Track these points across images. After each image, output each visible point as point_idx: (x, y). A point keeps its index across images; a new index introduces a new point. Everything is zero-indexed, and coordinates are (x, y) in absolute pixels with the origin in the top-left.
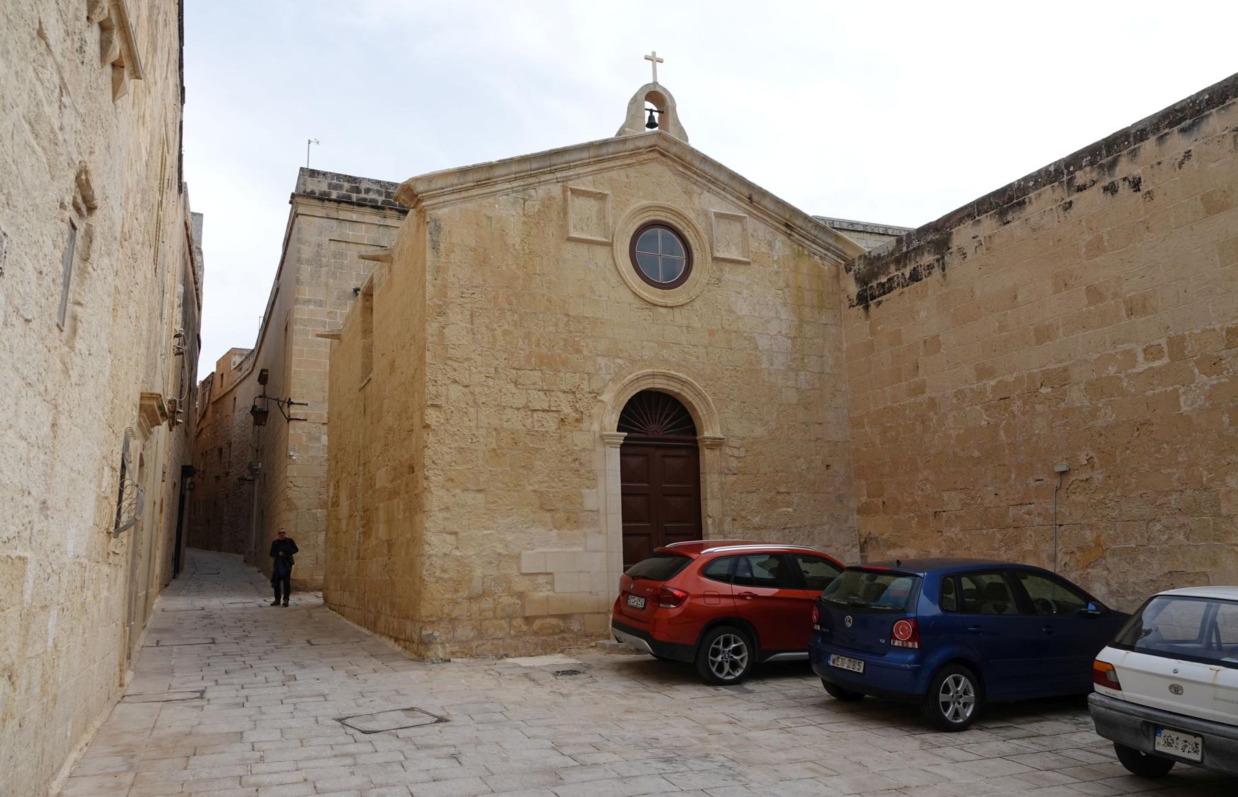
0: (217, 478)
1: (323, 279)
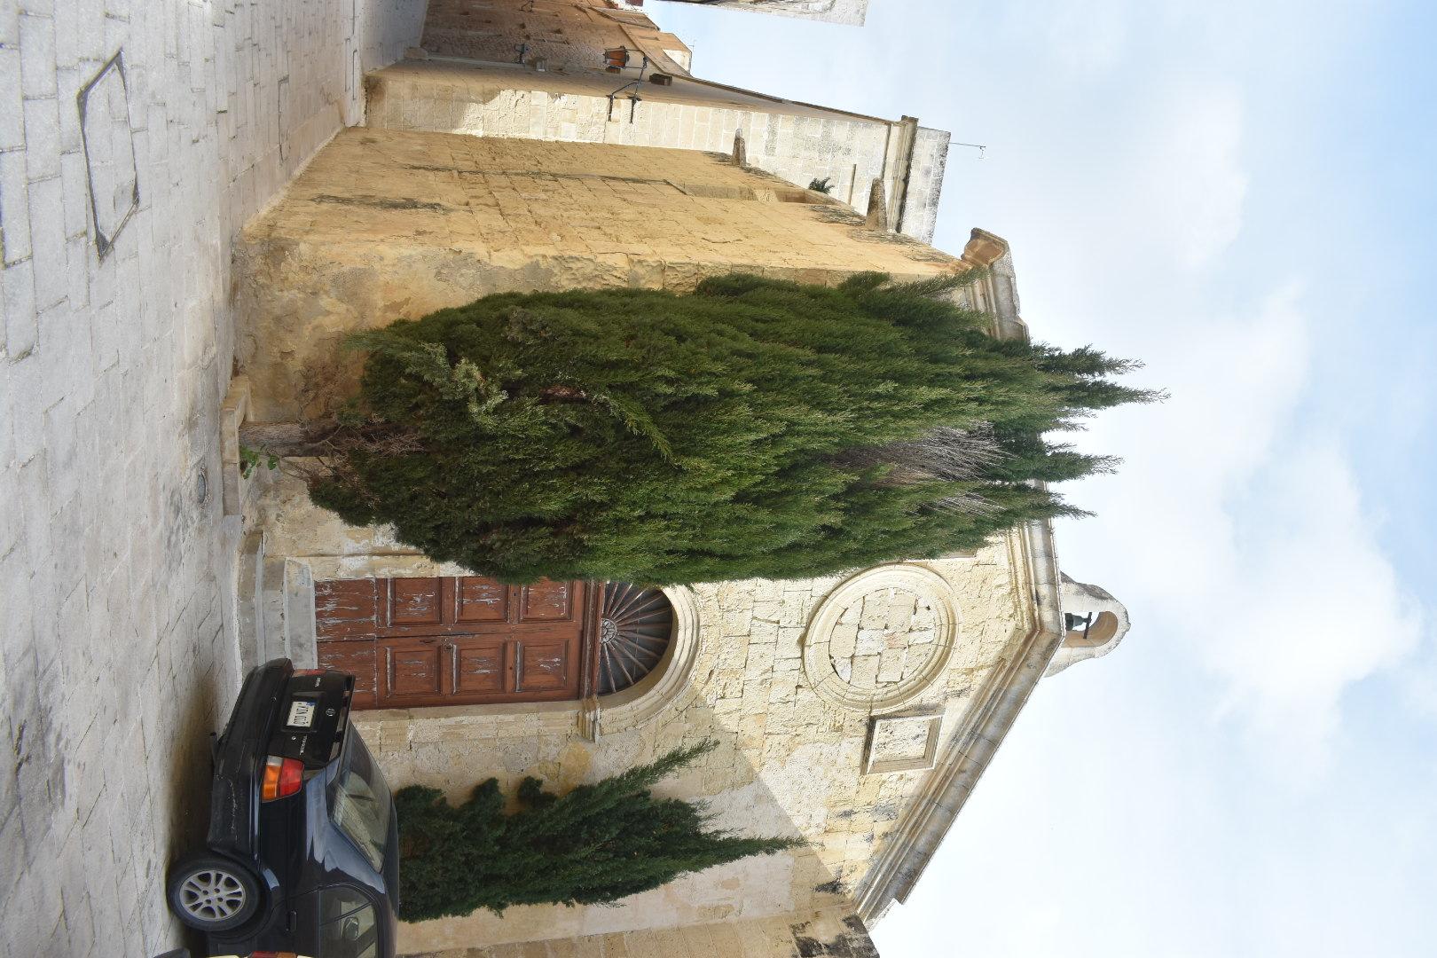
0: (523, 26)
1: (804, 153)
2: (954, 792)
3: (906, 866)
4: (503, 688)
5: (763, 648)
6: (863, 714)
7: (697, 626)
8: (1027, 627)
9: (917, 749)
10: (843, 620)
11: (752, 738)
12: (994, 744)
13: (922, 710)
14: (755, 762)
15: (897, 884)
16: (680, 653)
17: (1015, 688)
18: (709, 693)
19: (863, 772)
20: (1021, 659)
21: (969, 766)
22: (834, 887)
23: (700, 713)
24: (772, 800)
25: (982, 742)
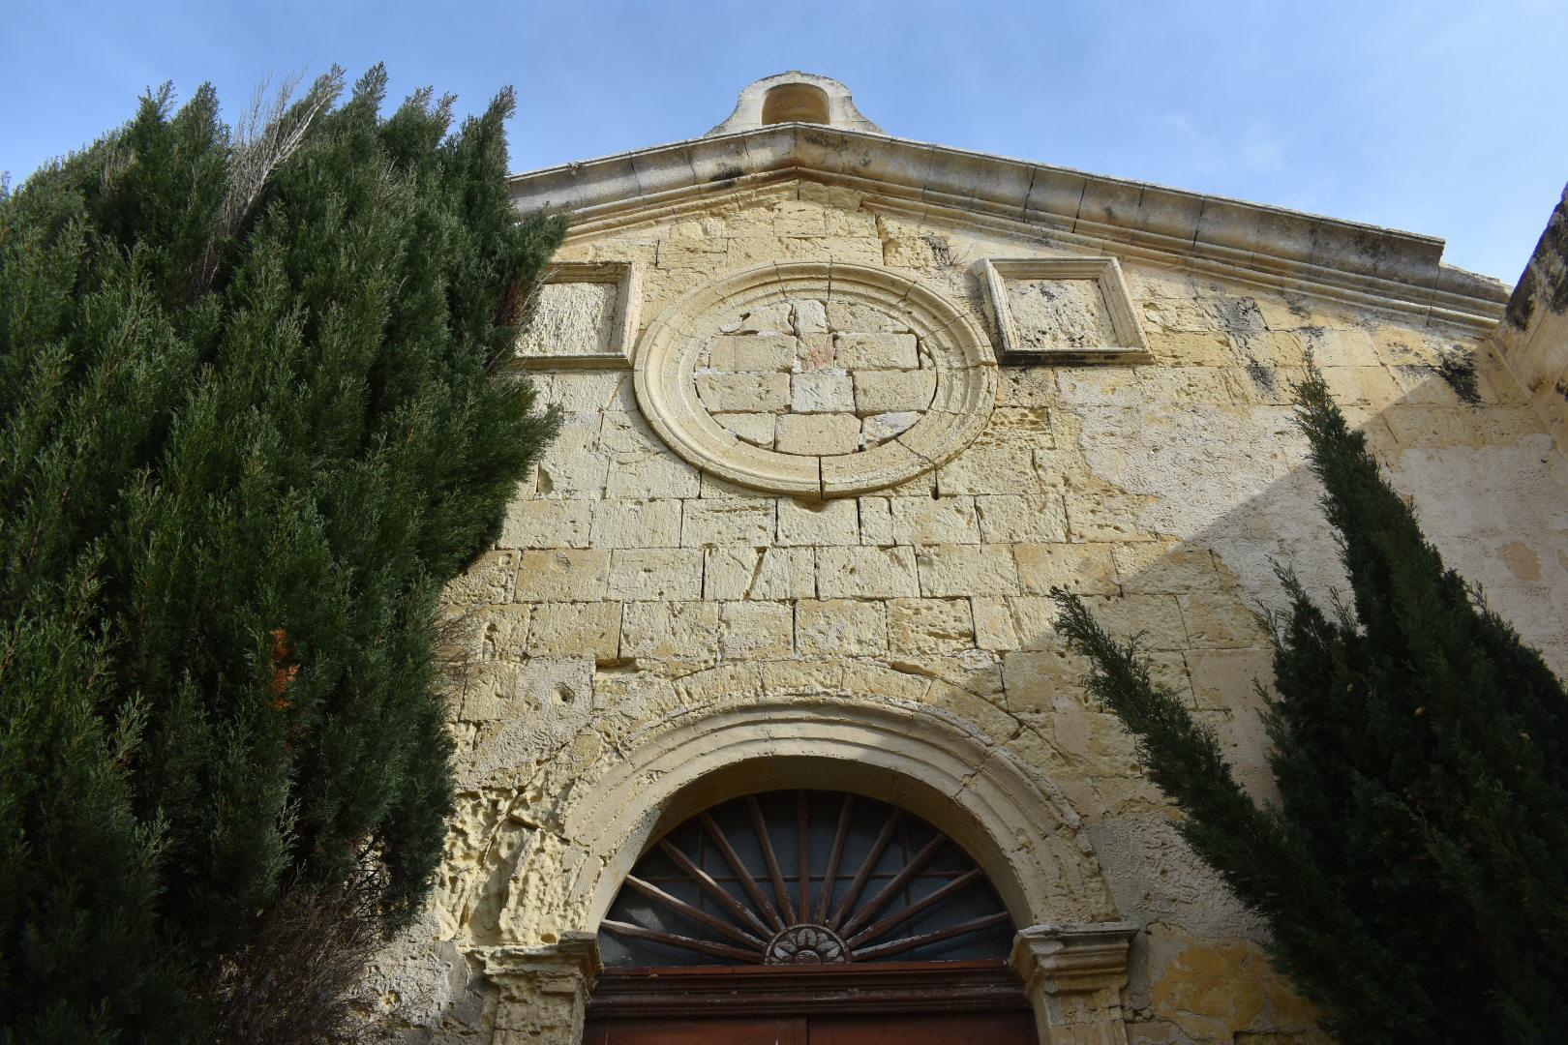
2: (1158, 217)
3: (1354, 259)
5: (830, 569)
6: (992, 376)
7: (759, 711)
11: (1086, 564)
12: (1034, 176)
13: (979, 292)
14: (1152, 552)
15: (1405, 266)
16: (847, 744)
17: (914, 172)
18: (953, 669)
19: (1141, 359)
20: (852, 179)
21: (1094, 206)
22: (1458, 376)
23: (1021, 678)
24: (1253, 507)
25: (1037, 196)
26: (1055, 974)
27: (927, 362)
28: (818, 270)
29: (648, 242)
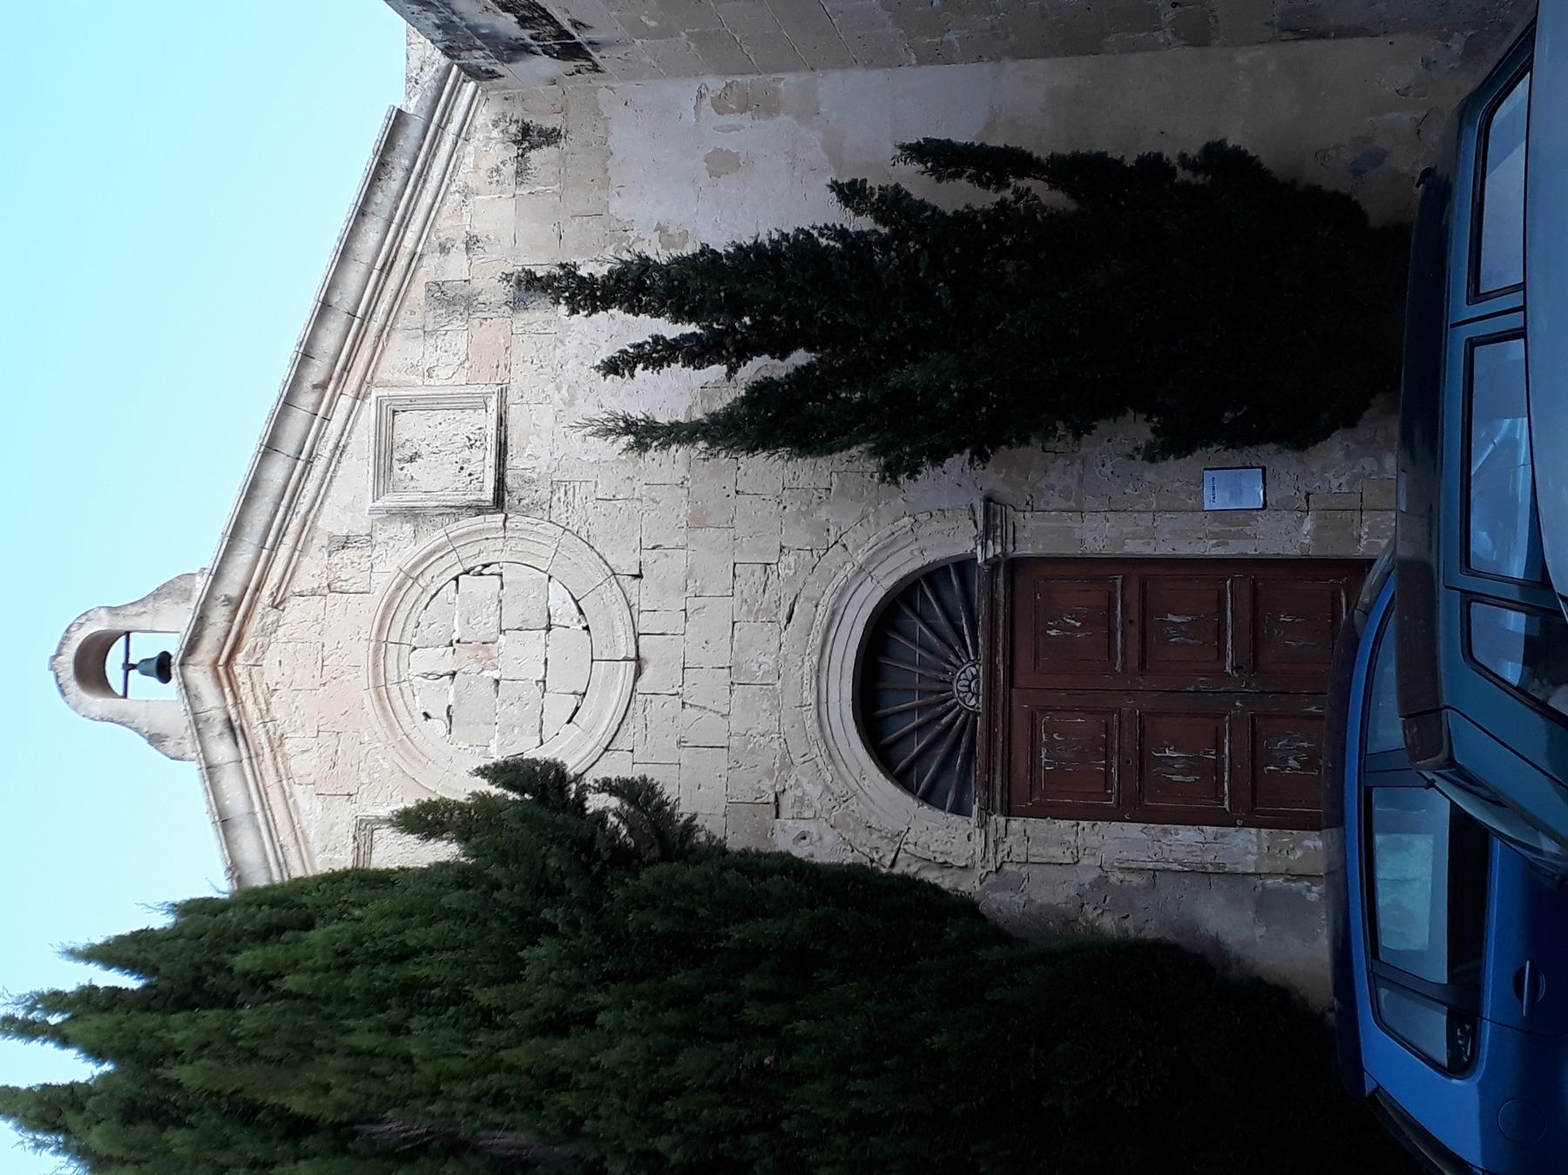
4: (1143, 585)
8: (239, 668)
9: (409, 427)
10: (572, 701)
21: (306, 399)
26: (1004, 548)
27: (494, 569)
28: (377, 651)
29: (318, 805)
